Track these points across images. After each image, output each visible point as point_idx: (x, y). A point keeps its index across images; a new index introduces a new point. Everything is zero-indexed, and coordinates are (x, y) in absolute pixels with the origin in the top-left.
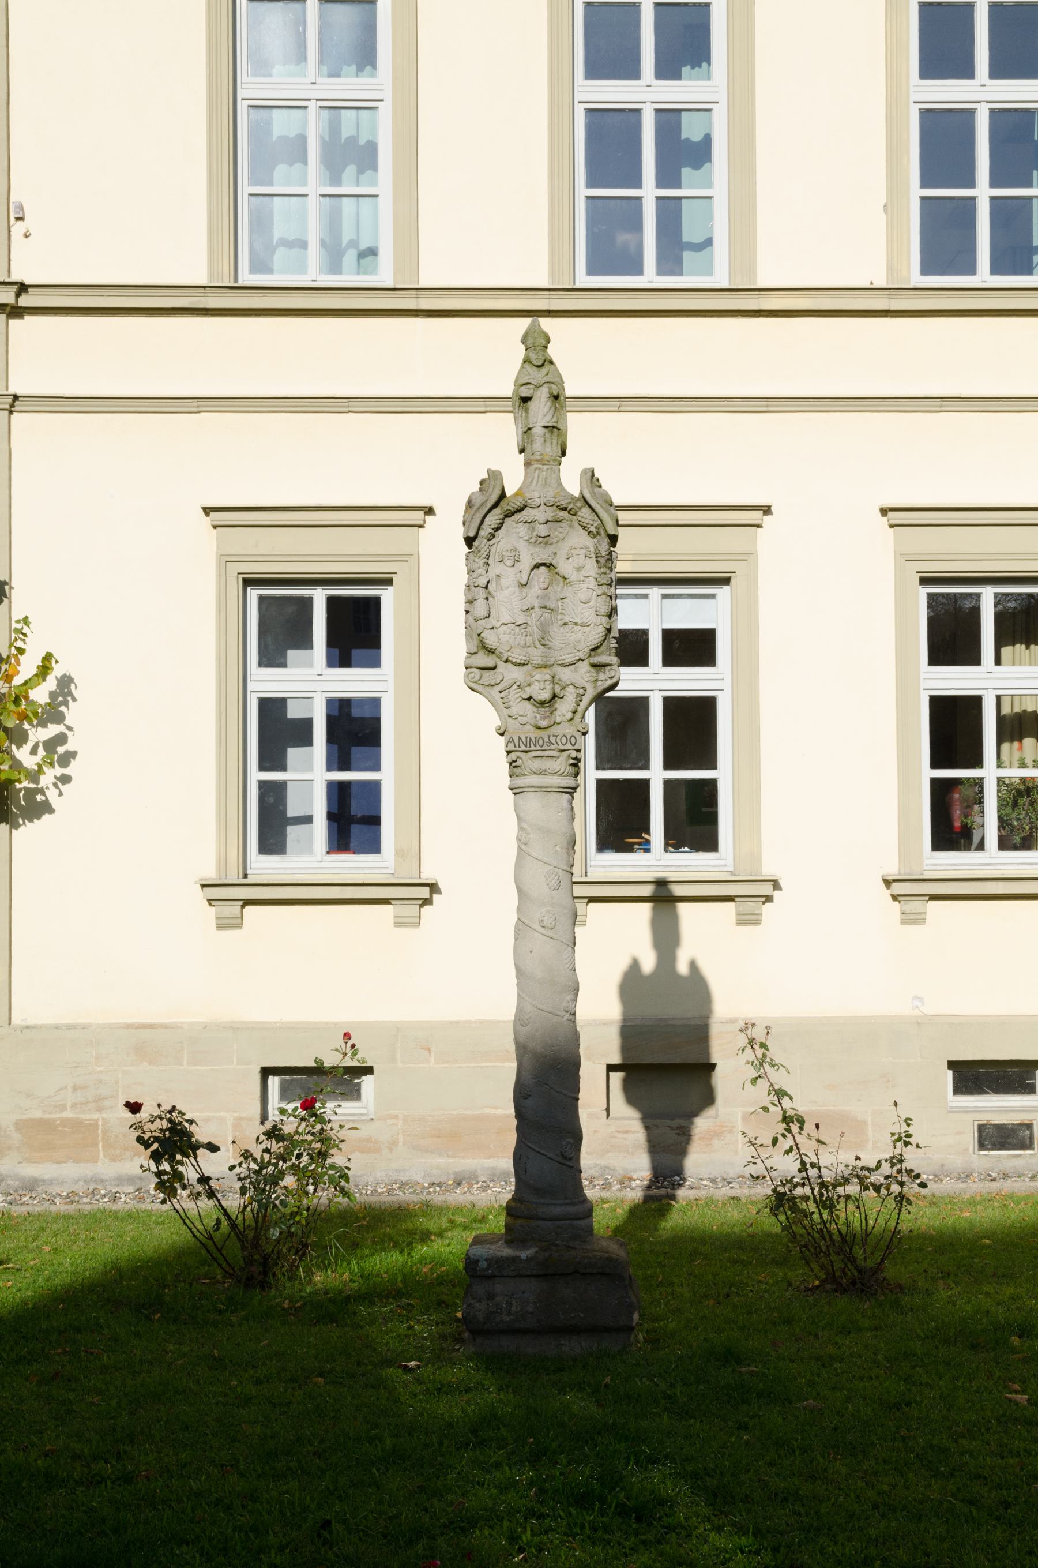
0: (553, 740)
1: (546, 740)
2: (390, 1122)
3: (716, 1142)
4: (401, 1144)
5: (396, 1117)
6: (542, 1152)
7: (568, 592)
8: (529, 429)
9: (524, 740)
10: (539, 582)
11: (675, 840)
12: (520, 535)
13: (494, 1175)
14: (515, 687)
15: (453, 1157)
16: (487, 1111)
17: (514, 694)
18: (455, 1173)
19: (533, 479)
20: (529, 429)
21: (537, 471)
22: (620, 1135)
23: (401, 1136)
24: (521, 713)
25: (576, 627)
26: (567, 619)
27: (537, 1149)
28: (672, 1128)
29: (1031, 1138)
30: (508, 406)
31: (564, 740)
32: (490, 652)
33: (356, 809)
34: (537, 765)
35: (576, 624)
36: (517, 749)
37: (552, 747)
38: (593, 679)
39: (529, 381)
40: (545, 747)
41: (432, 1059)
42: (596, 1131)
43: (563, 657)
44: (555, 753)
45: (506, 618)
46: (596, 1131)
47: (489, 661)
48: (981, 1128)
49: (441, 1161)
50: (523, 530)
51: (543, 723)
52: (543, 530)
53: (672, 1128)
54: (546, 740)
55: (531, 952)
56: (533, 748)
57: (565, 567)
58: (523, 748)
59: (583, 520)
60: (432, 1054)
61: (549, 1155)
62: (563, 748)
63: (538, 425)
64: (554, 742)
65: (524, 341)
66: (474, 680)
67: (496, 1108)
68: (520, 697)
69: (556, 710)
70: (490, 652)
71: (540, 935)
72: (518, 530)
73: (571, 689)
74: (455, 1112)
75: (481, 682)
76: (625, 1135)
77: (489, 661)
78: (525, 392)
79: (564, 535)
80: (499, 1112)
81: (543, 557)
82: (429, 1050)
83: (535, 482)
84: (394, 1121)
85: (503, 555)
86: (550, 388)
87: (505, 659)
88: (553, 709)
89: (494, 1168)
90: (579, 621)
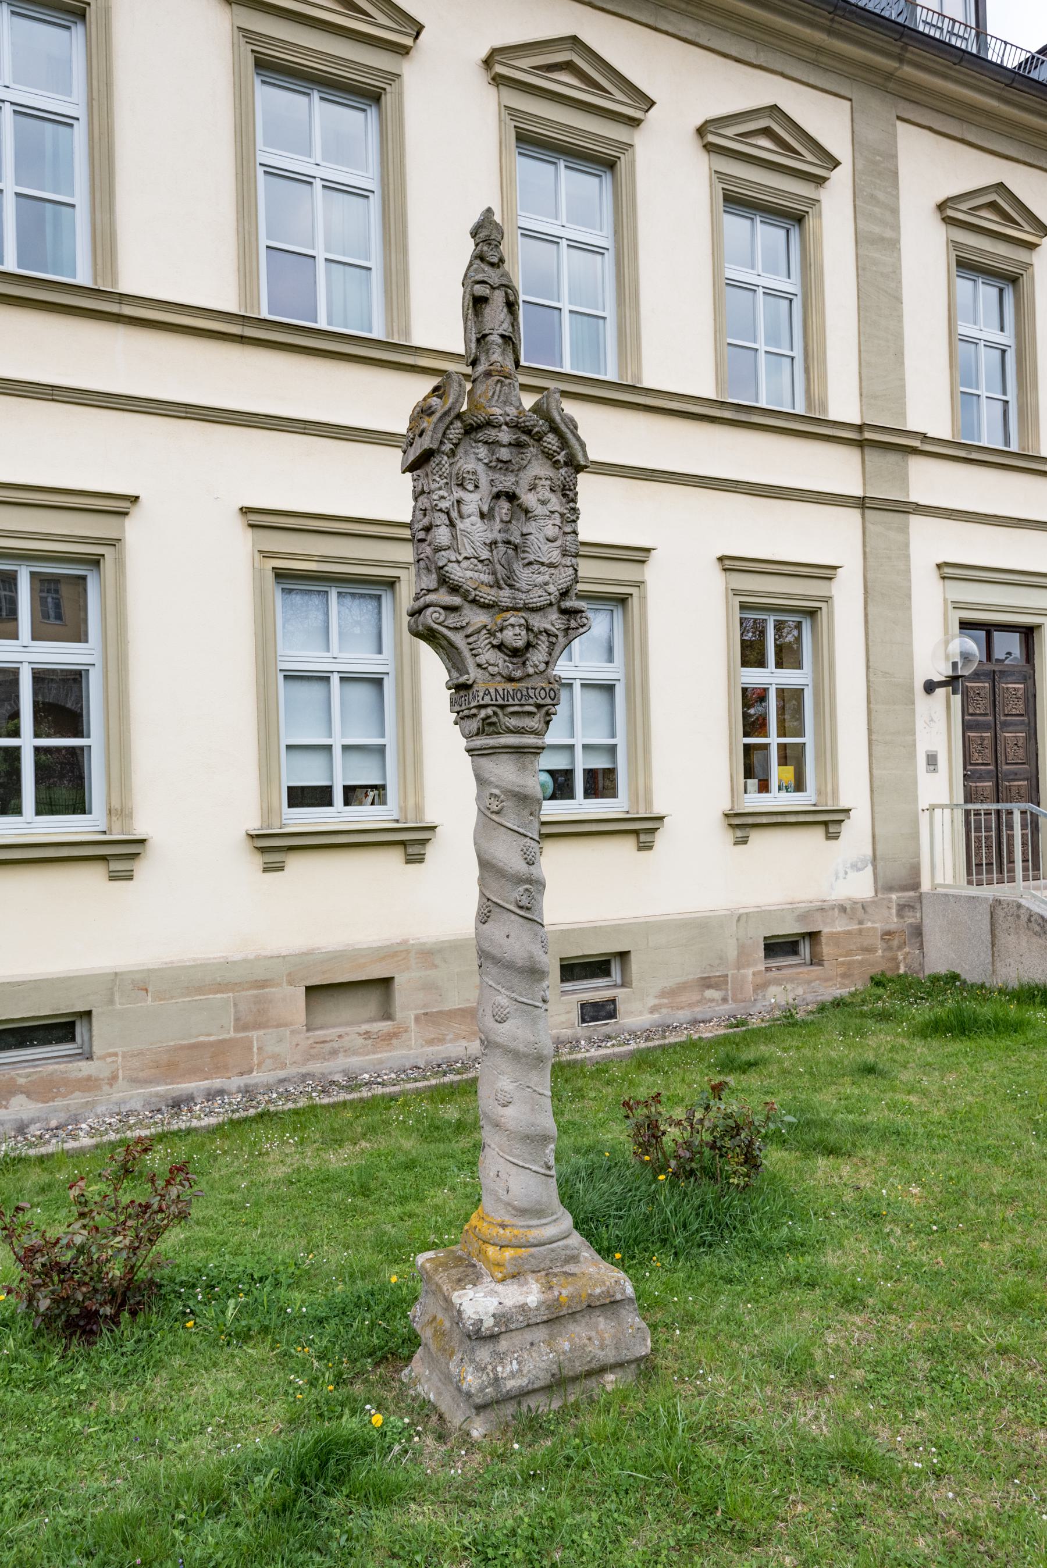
0: (531, 692)
1: (525, 693)
2: (109, 1060)
3: (394, 1041)
4: (121, 1078)
5: (116, 1054)
6: (527, 1166)
7: (531, 527)
8: (485, 336)
9: (501, 693)
10: (500, 513)
11: (46, 807)
12: (479, 456)
13: (209, 1095)
14: (485, 631)
15: (170, 1084)
16: (202, 1039)
17: (483, 640)
18: (173, 1098)
19: (494, 393)
20: (485, 336)
21: (499, 385)
22: (318, 1046)
23: (120, 1072)
24: (492, 662)
25: (542, 569)
26: (531, 557)
27: (521, 1164)
28: (360, 1034)
29: (615, 1010)
30: (912, 53)
31: (543, 693)
32: (455, 589)
33: (783, 760)
34: (513, 722)
35: (542, 564)
36: (494, 702)
37: (531, 701)
38: (563, 627)
39: (485, 279)
40: (523, 702)
41: (150, 999)
42: (297, 1045)
43: (535, 600)
44: (532, 709)
45: (469, 552)
46: (297, 1045)
47: (456, 600)
48: (583, 1006)
49: (161, 1089)
50: (482, 451)
51: (518, 674)
52: (504, 453)
53: (360, 1034)
54: (525, 693)
55: (508, 937)
56: (511, 702)
57: (529, 499)
58: (500, 702)
59: (549, 446)
60: (150, 994)
61: (534, 1168)
62: (542, 702)
63: (495, 332)
64: (532, 695)
65: (474, 234)
66: (438, 621)
67: (210, 1035)
68: (490, 643)
69: (527, 659)
70: (455, 589)
71: (517, 918)
72: (477, 451)
73: (544, 637)
74: (172, 1044)
75: (446, 624)
76: (322, 1045)
77: (456, 600)
78: (480, 290)
79: (525, 462)
80: (212, 1038)
81: (506, 482)
82: (147, 990)
83: (496, 397)
84: (113, 1058)
85: (463, 478)
86: (506, 294)
87: (470, 598)
88: (524, 658)
89: (208, 1089)
90: (545, 560)
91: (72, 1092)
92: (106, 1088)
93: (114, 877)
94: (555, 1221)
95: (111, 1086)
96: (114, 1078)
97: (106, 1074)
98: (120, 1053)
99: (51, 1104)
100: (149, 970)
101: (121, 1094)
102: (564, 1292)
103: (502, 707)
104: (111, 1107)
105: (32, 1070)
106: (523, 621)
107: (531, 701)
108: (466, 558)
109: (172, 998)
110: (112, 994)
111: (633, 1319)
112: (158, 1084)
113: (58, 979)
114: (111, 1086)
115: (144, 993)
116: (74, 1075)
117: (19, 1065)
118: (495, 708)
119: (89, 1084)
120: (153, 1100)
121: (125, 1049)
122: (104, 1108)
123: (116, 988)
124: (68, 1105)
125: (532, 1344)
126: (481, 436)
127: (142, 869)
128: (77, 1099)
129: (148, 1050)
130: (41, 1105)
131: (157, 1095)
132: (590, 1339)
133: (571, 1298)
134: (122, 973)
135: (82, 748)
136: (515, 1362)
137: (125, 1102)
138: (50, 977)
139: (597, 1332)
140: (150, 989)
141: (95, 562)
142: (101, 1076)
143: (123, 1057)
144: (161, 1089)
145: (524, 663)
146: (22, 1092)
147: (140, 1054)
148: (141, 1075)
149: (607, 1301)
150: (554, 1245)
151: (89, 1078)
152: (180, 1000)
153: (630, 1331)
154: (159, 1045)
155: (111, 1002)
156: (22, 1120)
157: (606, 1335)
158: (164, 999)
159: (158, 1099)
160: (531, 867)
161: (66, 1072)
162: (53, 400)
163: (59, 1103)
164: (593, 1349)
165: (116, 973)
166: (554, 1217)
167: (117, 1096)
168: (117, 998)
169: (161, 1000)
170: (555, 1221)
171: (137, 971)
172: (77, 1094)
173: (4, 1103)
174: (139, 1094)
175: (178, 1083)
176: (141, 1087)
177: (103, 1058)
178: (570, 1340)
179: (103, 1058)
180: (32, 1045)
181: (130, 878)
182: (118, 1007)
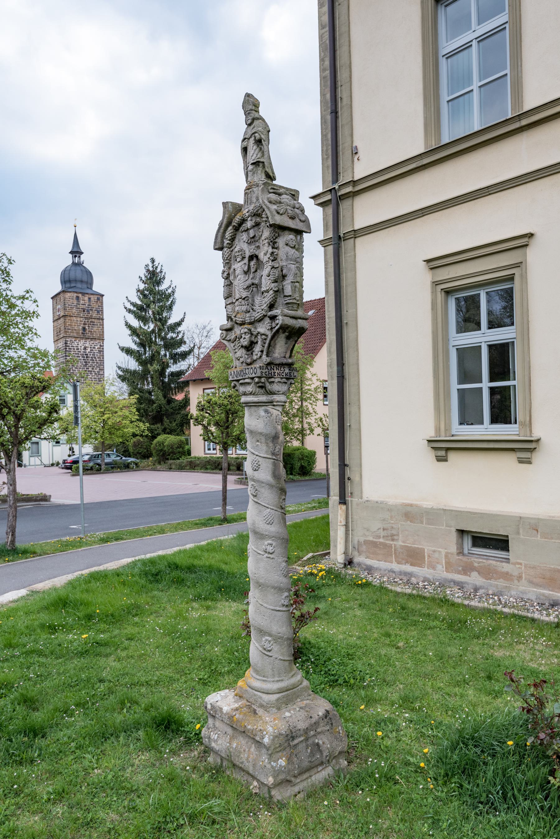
2: (518, 566)
4: (524, 578)
5: (521, 564)
11: (495, 420)
18: (553, 600)
23: (523, 575)
38: (270, 327)
41: (539, 536)
45: (237, 296)
49: (546, 592)
58: (235, 378)
60: (539, 533)
74: (553, 567)
91: (499, 578)
92: (516, 581)
93: (521, 461)
94: (264, 681)
95: (519, 581)
96: (520, 578)
97: (516, 573)
98: (523, 564)
99: (489, 581)
100: (538, 519)
101: (524, 588)
102: (237, 716)
103: (238, 381)
104: (519, 593)
105: (481, 560)
106: (246, 330)
107: (247, 376)
108: (237, 300)
109: (552, 538)
110: (519, 529)
111: (266, 759)
112: (544, 588)
113: (492, 514)
114: (519, 581)
115: (536, 532)
116: (500, 569)
117: (482, 557)
118: (234, 382)
119: (507, 576)
120: (542, 597)
121: (526, 562)
122: (515, 593)
123: (521, 526)
124: (497, 585)
125: (226, 733)
126: (242, 229)
127: (537, 457)
128: (501, 583)
129: (539, 566)
130: (484, 580)
131: (543, 595)
132: (244, 751)
133: (238, 721)
134: (524, 518)
135: (509, 387)
136: (217, 735)
137: (526, 593)
138: (488, 512)
139: (249, 751)
140: (539, 530)
141: (511, 278)
142: (514, 574)
143: (525, 567)
144: (546, 592)
145: (252, 354)
146: (476, 571)
147: (534, 568)
148: (534, 580)
149: (252, 736)
150: (256, 693)
151: (507, 573)
152: (557, 541)
153: (261, 763)
154: (545, 565)
155: (518, 533)
156: (476, 586)
157: (251, 756)
158: (548, 538)
159: (544, 598)
160: (255, 472)
161: (496, 566)
162: (490, 194)
163: (492, 582)
164: (244, 756)
165: (520, 517)
166: (264, 679)
167: (522, 588)
168: (521, 531)
169: (545, 538)
170: (264, 681)
171: (532, 518)
172: (501, 580)
173: (469, 573)
174: (534, 591)
175: (556, 592)
176: (535, 588)
177: (515, 564)
178: (238, 744)
179: (515, 564)
180: (489, 548)
181: (530, 463)
182: (522, 537)
